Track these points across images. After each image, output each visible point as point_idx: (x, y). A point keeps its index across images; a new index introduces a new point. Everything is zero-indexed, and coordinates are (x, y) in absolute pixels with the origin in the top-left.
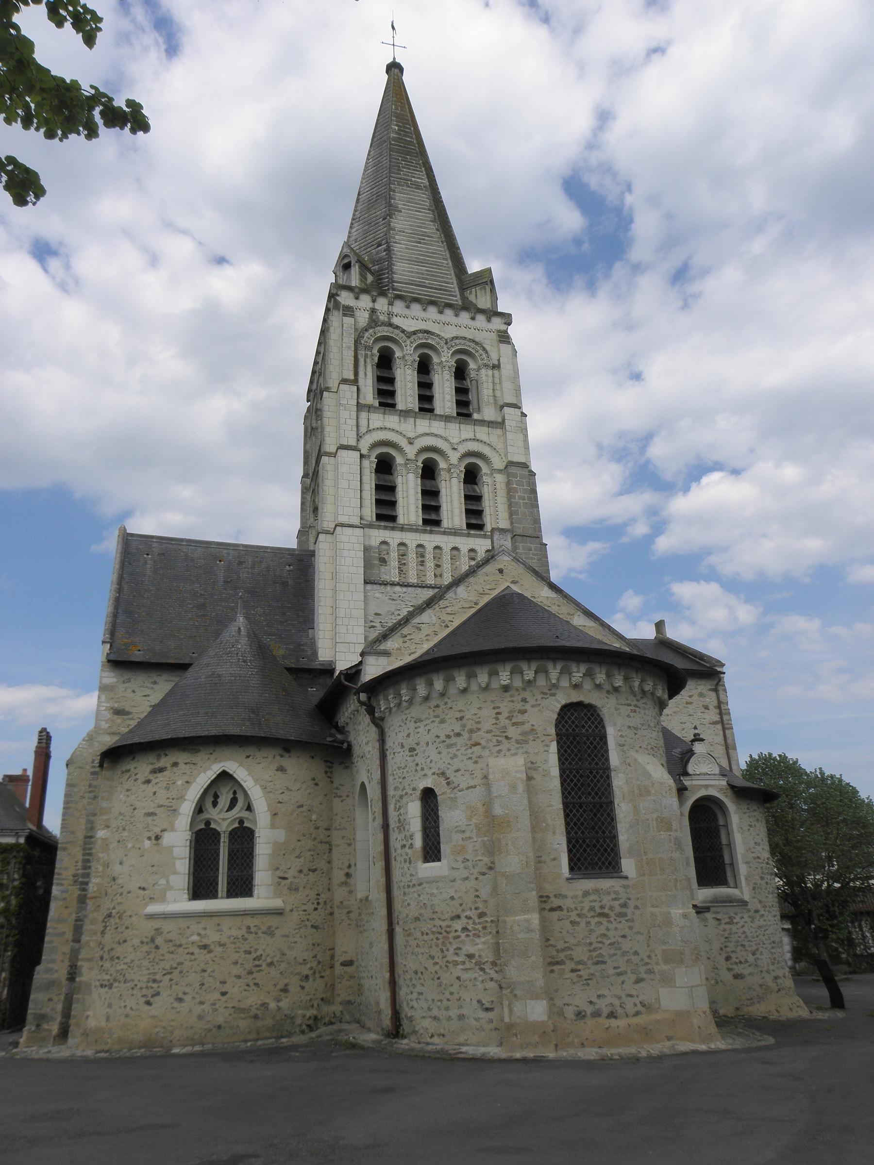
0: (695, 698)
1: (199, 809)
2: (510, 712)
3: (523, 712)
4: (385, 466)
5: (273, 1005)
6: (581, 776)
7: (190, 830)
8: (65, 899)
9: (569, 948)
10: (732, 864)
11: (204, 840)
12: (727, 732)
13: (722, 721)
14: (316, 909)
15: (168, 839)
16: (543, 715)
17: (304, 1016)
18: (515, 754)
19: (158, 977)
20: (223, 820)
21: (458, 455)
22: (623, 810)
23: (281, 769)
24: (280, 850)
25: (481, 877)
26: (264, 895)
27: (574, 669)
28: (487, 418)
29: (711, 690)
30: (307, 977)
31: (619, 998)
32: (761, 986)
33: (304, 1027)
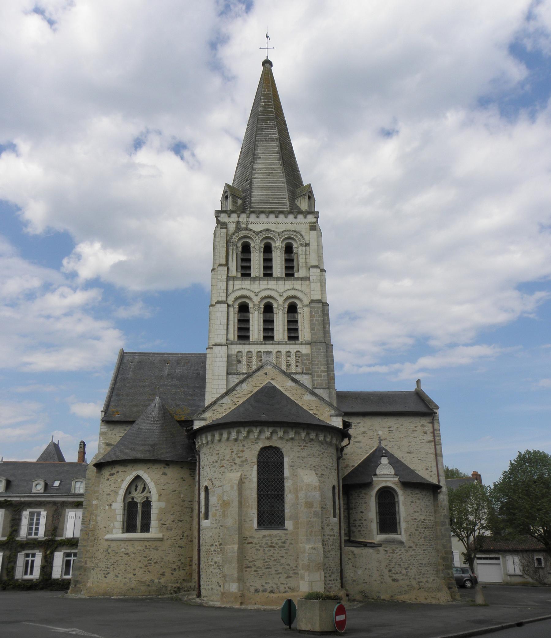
0: (419, 428)
1: (128, 491)
2: (237, 451)
3: (243, 451)
4: (244, 308)
5: (156, 581)
6: (269, 482)
7: (124, 501)
8: (86, 530)
9: (254, 561)
10: (399, 522)
11: (130, 507)
12: (437, 447)
13: (434, 441)
14: (181, 539)
15: (114, 506)
16: (252, 452)
17: (172, 587)
18: (238, 471)
19: (109, 566)
20: (139, 497)
21: (283, 299)
22: (289, 498)
23: (165, 474)
24: (162, 511)
25: (221, 528)
26: (154, 532)
27: (266, 430)
28: (301, 276)
29: (429, 423)
30: (175, 569)
31: (277, 584)
32: (408, 586)
33: (172, 591)
